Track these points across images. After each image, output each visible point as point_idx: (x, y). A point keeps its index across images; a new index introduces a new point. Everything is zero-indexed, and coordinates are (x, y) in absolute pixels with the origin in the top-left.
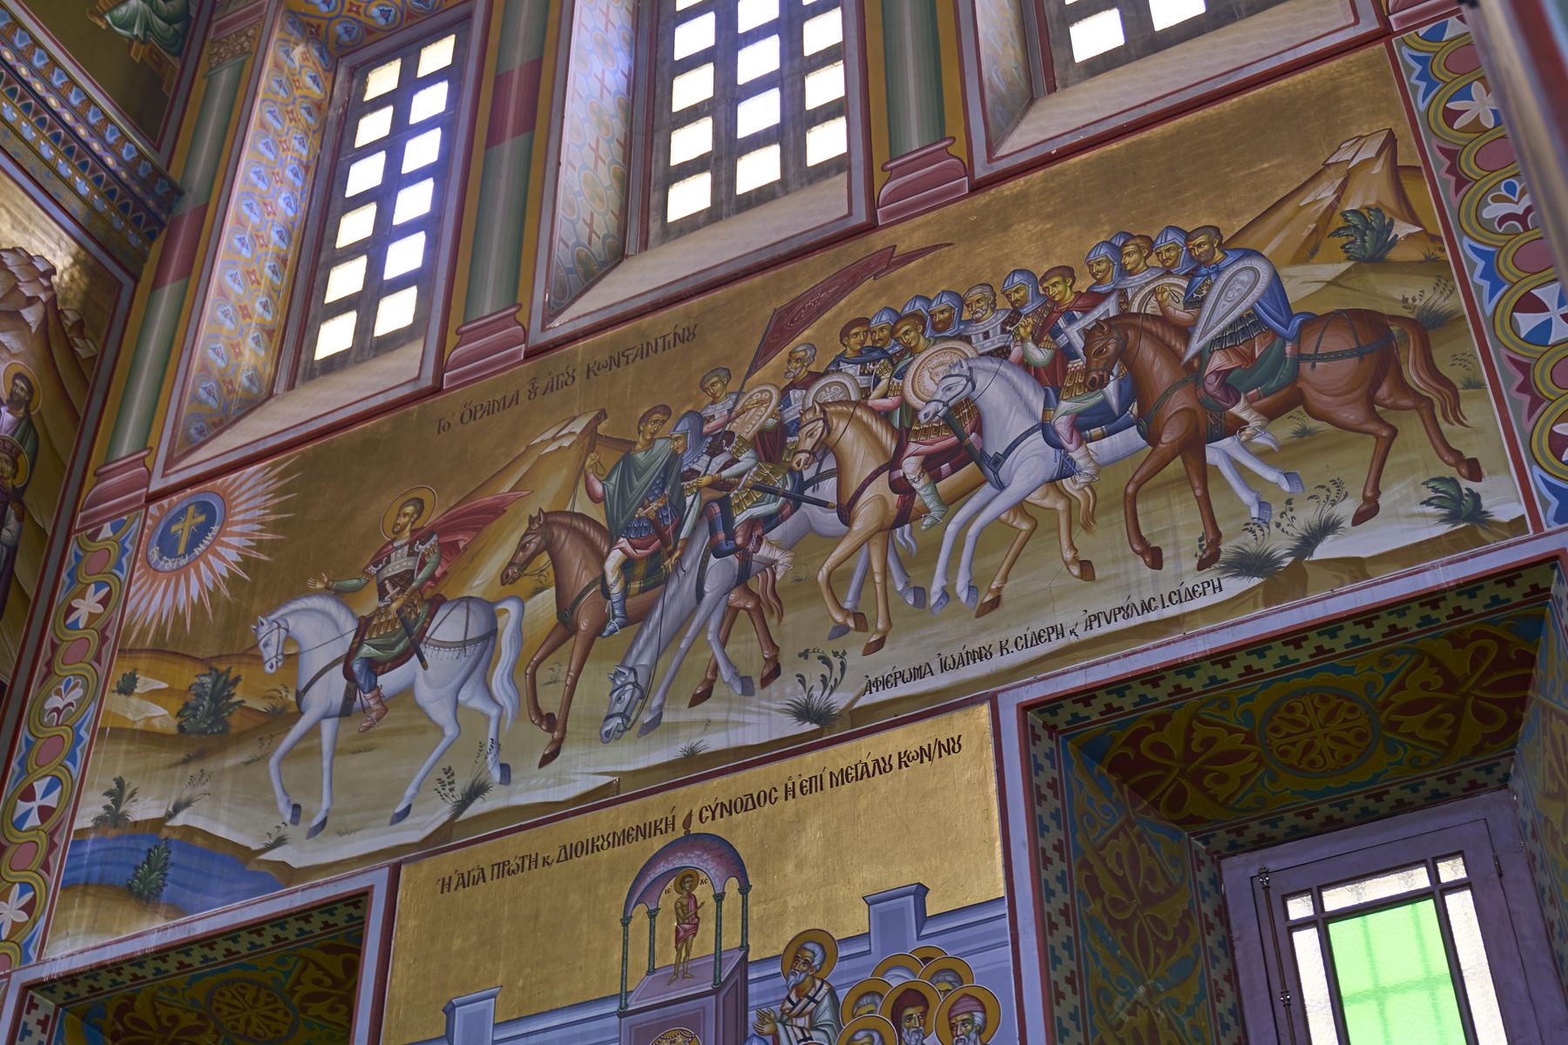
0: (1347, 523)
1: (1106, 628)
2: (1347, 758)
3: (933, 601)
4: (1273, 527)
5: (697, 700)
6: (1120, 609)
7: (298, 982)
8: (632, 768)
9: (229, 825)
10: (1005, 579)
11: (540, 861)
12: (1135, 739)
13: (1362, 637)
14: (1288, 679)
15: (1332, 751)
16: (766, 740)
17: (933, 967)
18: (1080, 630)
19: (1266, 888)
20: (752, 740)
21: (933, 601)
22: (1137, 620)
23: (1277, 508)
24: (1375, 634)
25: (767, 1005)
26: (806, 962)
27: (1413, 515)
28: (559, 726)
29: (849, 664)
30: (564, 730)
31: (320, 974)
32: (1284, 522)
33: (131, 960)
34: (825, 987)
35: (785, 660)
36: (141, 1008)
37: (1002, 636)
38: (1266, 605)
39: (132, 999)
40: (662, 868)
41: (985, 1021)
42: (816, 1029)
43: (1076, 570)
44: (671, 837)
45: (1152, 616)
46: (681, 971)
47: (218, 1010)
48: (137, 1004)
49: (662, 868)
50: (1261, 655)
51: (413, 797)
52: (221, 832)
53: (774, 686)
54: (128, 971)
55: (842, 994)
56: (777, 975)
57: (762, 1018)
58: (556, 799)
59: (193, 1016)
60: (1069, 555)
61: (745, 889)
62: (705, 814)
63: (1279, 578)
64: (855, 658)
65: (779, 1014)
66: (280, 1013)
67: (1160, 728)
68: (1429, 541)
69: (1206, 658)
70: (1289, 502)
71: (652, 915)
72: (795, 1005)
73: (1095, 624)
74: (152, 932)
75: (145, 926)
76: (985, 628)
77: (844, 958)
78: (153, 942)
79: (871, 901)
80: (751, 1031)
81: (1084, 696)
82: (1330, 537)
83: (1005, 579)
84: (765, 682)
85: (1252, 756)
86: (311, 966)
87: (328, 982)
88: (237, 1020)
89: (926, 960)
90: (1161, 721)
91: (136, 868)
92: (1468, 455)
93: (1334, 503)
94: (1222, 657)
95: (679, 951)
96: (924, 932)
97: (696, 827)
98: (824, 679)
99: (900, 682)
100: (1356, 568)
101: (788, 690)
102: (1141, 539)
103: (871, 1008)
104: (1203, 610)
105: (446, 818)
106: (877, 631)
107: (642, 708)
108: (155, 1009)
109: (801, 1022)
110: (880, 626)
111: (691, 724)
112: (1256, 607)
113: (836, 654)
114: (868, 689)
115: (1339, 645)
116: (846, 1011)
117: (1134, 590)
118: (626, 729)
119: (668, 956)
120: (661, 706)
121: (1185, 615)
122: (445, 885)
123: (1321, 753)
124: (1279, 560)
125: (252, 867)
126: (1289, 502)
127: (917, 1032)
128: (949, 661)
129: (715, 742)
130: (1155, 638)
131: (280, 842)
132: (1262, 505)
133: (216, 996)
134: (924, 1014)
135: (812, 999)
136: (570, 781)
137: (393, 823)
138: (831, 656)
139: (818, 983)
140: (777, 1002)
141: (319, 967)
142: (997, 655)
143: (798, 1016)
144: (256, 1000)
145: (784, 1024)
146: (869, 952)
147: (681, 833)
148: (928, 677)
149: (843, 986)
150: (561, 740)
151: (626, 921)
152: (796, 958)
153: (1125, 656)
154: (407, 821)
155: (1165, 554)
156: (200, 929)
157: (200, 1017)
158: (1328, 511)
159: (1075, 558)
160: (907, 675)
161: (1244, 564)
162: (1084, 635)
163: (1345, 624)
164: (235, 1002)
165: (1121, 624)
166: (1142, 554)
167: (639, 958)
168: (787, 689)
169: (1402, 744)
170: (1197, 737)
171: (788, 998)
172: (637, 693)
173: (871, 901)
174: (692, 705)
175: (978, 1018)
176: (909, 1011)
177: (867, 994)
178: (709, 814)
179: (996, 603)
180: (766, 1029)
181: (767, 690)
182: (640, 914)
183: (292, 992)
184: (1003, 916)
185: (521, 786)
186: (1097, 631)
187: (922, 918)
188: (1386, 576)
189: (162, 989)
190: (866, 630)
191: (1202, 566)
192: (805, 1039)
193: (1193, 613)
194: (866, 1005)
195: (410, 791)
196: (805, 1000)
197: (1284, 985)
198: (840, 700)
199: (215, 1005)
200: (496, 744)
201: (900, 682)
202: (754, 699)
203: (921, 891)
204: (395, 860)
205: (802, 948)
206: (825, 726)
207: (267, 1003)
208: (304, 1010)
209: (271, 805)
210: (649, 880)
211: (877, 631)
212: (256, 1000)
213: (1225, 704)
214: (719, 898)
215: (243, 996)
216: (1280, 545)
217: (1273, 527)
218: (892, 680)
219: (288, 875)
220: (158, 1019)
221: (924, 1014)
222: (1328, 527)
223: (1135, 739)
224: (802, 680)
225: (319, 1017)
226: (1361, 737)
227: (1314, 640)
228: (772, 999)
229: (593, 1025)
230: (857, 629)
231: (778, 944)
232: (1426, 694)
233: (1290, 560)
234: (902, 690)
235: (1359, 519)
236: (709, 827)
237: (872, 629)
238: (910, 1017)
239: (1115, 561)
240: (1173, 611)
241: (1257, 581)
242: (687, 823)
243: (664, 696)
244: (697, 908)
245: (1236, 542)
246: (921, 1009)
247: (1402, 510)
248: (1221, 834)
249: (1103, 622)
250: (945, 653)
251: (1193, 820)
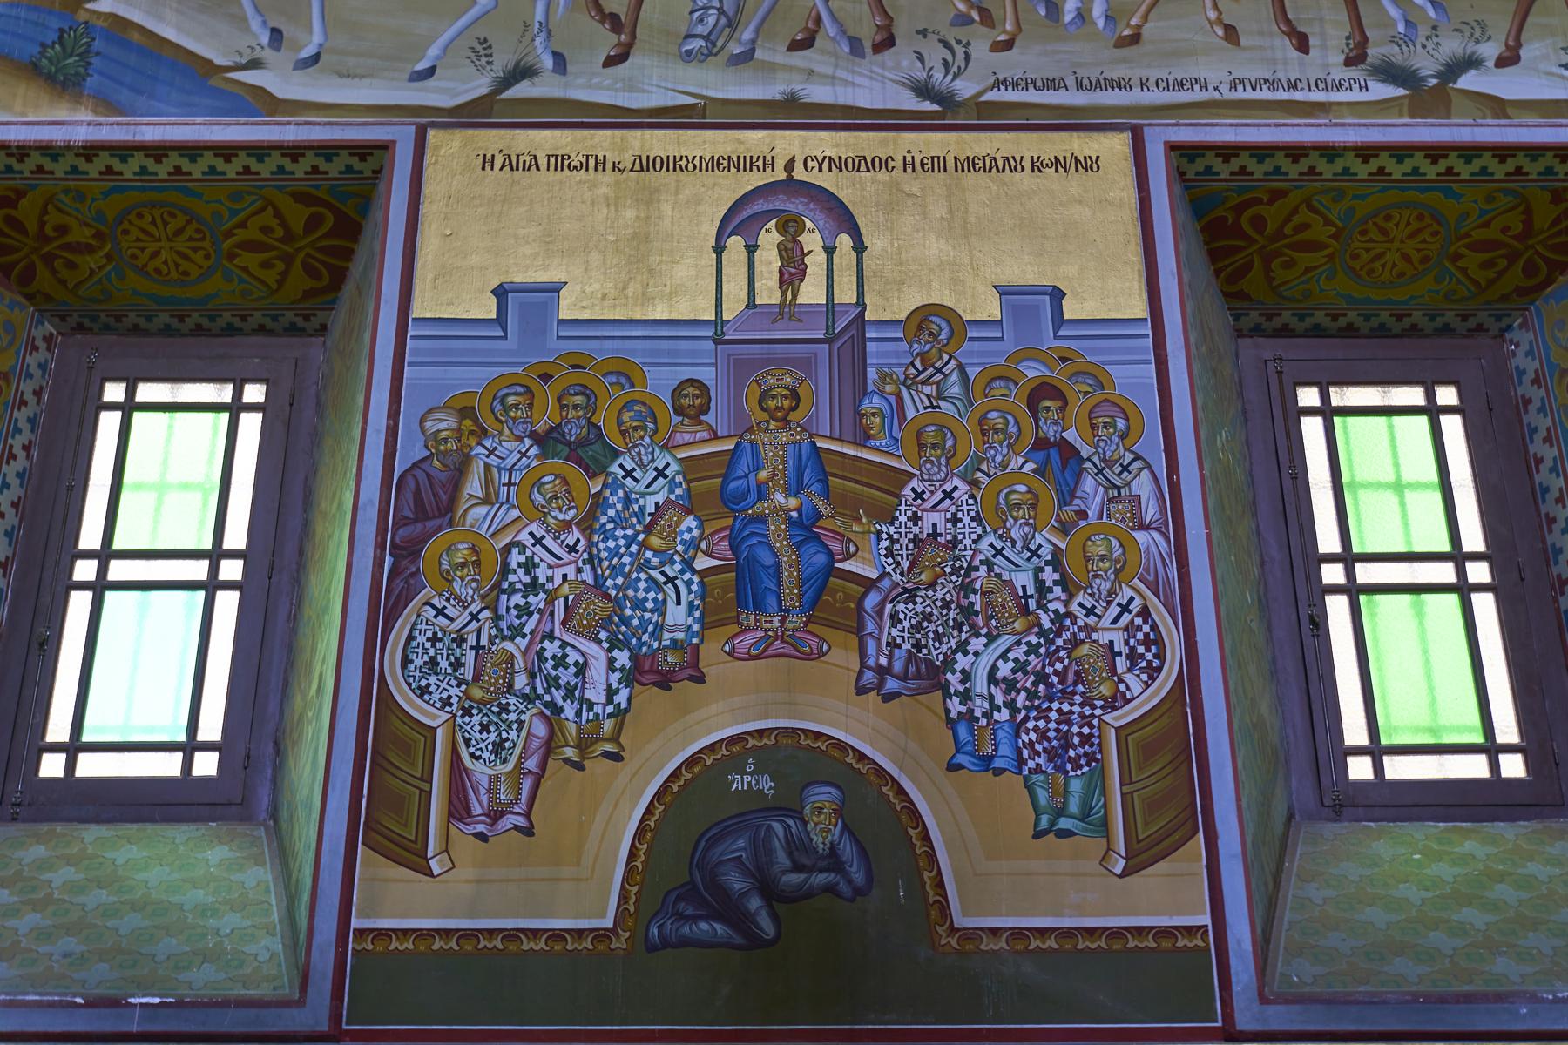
0: (1491, 64)
1: (1250, 95)
2: (1402, 275)
3: (1068, 18)
4: (1419, 47)
5: (795, 46)
6: (1266, 81)
7: (243, 225)
8: (720, 95)
9: (179, 29)
10: (1145, 18)
11: (609, 166)
12: (1240, 209)
13: (253, 169)
14: (1403, 190)
15: (1394, 265)
16: (881, 107)
17: (1072, 368)
18: (1224, 88)
19: (1280, 373)
20: (863, 103)
21: (1068, 18)
22: (1281, 95)
23: (1423, 31)
24: (231, 169)
25: (890, 366)
26: (931, 334)
27: (1552, 74)
28: (627, 30)
29: (974, 55)
30: (633, 36)
31: (274, 223)
32: (1430, 46)
33: (47, 149)
34: (953, 363)
35: (901, 29)
36: (27, 210)
37: (1144, 73)
38: (1412, 116)
39: (20, 194)
40: (760, 206)
41: (1128, 428)
42: (944, 399)
43: (1220, 32)
44: (768, 177)
45: (1298, 96)
46: (788, 311)
47: (125, 232)
48: (24, 203)
49: (760, 206)
50: (193, 159)
51: (438, 58)
52: (169, 33)
53: (888, 55)
54: (35, 159)
55: (972, 373)
56: (900, 339)
57: (883, 377)
58: (626, 105)
59: (88, 232)
60: (1212, 15)
61: (859, 247)
62: (810, 164)
63: (1429, 97)
64: (980, 49)
65: (902, 378)
66: (202, 253)
67: (1271, 202)
68: (1557, 102)
69: (1355, 148)
70: (1435, 28)
71: (751, 249)
72: (920, 373)
73: (1240, 88)
74: (80, 123)
75: (62, 114)
76: (1125, 60)
77: (972, 339)
78: (81, 135)
79: (1004, 292)
80: (870, 387)
81: (1228, 152)
82: (1473, 72)
83: (1145, 18)
84: (878, 48)
85: (1326, 252)
86: (270, 210)
87: (280, 232)
88: (143, 250)
89: (1064, 359)
90: (1277, 195)
91: (43, 45)
92: (1301, 29)
93: (1477, 42)
94: (1366, 152)
95: (784, 294)
96: (1061, 333)
97: (799, 174)
98: (945, 63)
99: (1031, 87)
100: (1498, 107)
101: (905, 63)
102: (1288, 21)
103: (1004, 391)
104: (1349, 104)
105: (484, 91)
106: (1005, 32)
107: (730, 37)
108: (45, 212)
109: (927, 389)
110: (1008, 27)
111: (791, 69)
112: (1401, 115)
113: (959, 42)
114: (997, 84)
115: (197, 170)
116: (978, 389)
117: (1279, 67)
118: (710, 54)
119: (769, 291)
120: (753, 41)
121: (1331, 104)
122: (487, 162)
123: (1383, 266)
124: (1424, 79)
125: (214, 82)
126: (1435, 28)
127: (1056, 424)
128: (1086, 82)
129: (819, 94)
130: (1300, 117)
131: (255, 64)
132: (1408, 23)
133: (132, 217)
134: (1063, 409)
135: (939, 371)
136: (644, 91)
137: (411, 80)
138: (953, 43)
139: (946, 357)
140: (899, 365)
141: (278, 214)
142: (1137, 89)
143: (924, 383)
144: (179, 232)
145: (908, 388)
146: (1001, 339)
147: (783, 176)
148: (1062, 91)
149: (973, 365)
150: (630, 45)
151: (719, 249)
152: (920, 328)
153: (1277, 125)
154: (431, 83)
155: (1311, 42)
156: (151, 133)
157: (99, 235)
158: (1471, 47)
159: (1219, 21)
160: (1039, 84)
161: (1390, 73)
162: (1228, 95)
163: (342, 152)
164: (152, 229)
165: (1265, 94)
166: (1289, 35)
167: (735, 291)
168: (901, 61)
169: (1451, 275)
170: (1296, 220)
171: (912, 364)
172: (723, 21)
173: (1004, 292)
174: (790, 49)
175: (1121, 424)
176: (1047, 403)
177: (1000, 378)
178: (815, 164)
179: (1135, 39)
180: (888, 388)
181: (879, 57)
182: (735, 243)
183: (229, 234)
184: (410, 364)
185: (580, 81)
186: (1240, 95)
187: (1059, 320)
188: (1531, 121)
189: (67, 191)
190: (993, 26)
191: (1349, 62)
192: (932, 406)
193: (1340, 104)
194: (999, 388)
195: (433, 51)
196: (931, 371)
197: (1292, 461)
198: (965, 88)
199: (126, 225)
200: (546, 28)
201: (1031, 87)
202: (865, 62)
203: (1057, 295)
204: (424, 120)
205: (926, 319)
206: (947, 112)
207: (191, 239)
208: (231, 257)
209: (241, 22)
210: (745, 214)
211: (1005, 32)
212: (179, 232)
213: (1340, 195)
214: (830, 250)
215: (165, 224)
216: (1427, 65)
217: (1419, 47)
218: (1023, 84)
219: (268, 104)
220: (42, 224)
221: (1063, 409)
222: (1472, 62)
223: (1240, 209)
224: (921, 58)
225: (245, 269)
226: (1425, 260)
227: (174, 159)
228: (894, 361)
229: (665, 345)
230: (982, 23)
231: (900, 309)
232: (1502, 237)
233: (1434, 81)
234: (1032, 96)
235: (1501, 63)
236: (826, 180)
237: (999, 28)
238: (1048, 409)
239: (1261, 33)
240: (1318, 96)
241: (1402, 92)
242: (790, 166)
243: (757, 31)
244: (804, 255)
245: (1383, 50)
246: (1059, 403)
247: (1542, 67)
248: (1254, 314)
249: (1248, 88)
250: (1081, 73)
251: (1242, 296)
